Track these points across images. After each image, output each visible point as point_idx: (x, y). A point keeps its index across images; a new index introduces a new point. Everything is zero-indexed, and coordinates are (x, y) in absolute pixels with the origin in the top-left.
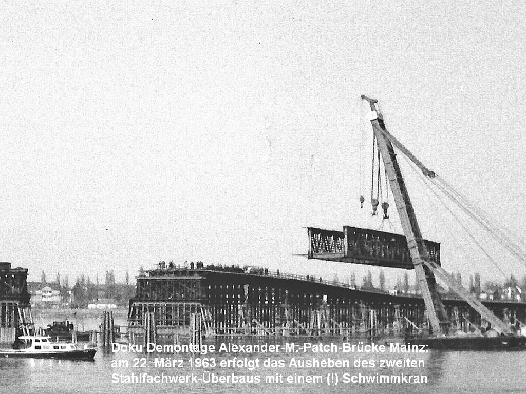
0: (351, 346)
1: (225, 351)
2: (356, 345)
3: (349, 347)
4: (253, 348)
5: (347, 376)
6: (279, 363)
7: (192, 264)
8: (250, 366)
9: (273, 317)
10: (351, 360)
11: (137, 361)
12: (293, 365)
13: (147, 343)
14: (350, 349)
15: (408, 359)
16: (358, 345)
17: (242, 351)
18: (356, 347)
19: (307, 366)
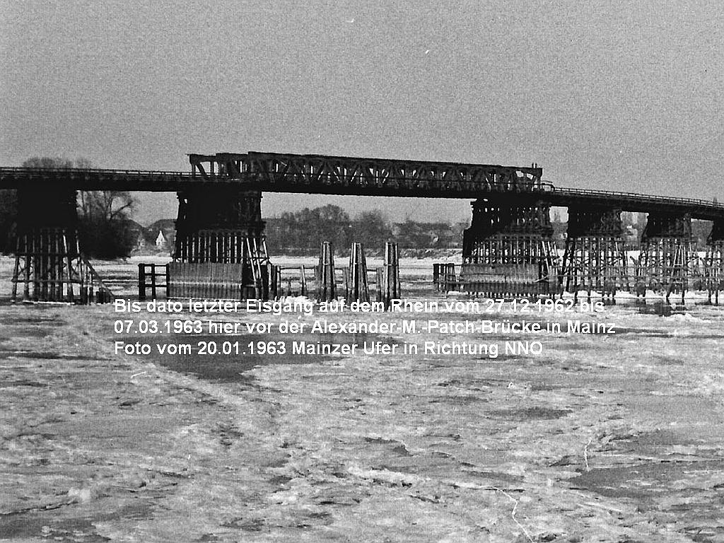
0: (126, 304)
1: (319, 331)
2: (500, 324)
3: (123, 305)
4: (478, 348)
5: (267, 309)
6: (270, 308)
7: (533, 165)
8: (276, 310)
9: (397, 291)
10: (50, 271)
11: (203, 345)
12: (317, 329)
13: (567, 347)
14: (125, 307)
15: (464, 343)
16: (503, 324)
17: (343, 332)
18: (501, 326)
19: (264, 310)
